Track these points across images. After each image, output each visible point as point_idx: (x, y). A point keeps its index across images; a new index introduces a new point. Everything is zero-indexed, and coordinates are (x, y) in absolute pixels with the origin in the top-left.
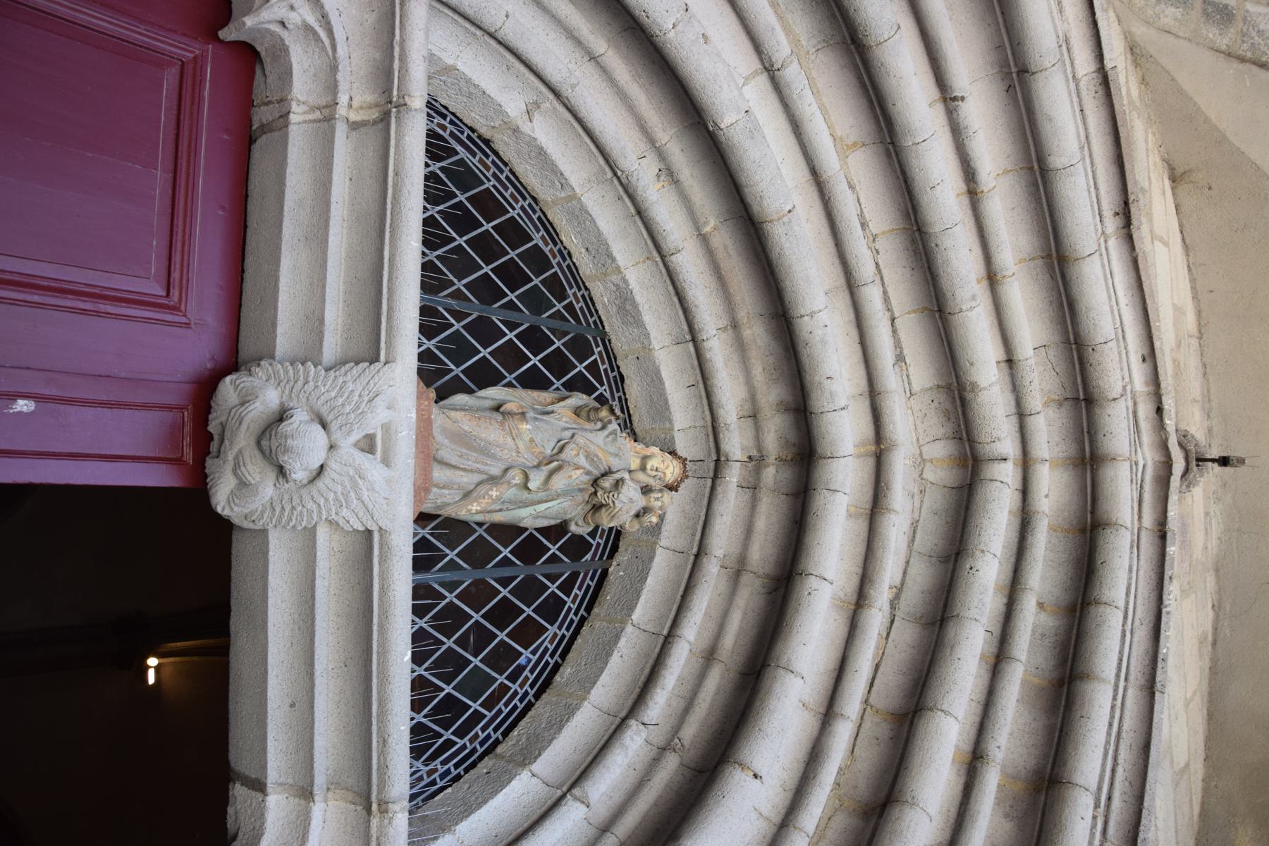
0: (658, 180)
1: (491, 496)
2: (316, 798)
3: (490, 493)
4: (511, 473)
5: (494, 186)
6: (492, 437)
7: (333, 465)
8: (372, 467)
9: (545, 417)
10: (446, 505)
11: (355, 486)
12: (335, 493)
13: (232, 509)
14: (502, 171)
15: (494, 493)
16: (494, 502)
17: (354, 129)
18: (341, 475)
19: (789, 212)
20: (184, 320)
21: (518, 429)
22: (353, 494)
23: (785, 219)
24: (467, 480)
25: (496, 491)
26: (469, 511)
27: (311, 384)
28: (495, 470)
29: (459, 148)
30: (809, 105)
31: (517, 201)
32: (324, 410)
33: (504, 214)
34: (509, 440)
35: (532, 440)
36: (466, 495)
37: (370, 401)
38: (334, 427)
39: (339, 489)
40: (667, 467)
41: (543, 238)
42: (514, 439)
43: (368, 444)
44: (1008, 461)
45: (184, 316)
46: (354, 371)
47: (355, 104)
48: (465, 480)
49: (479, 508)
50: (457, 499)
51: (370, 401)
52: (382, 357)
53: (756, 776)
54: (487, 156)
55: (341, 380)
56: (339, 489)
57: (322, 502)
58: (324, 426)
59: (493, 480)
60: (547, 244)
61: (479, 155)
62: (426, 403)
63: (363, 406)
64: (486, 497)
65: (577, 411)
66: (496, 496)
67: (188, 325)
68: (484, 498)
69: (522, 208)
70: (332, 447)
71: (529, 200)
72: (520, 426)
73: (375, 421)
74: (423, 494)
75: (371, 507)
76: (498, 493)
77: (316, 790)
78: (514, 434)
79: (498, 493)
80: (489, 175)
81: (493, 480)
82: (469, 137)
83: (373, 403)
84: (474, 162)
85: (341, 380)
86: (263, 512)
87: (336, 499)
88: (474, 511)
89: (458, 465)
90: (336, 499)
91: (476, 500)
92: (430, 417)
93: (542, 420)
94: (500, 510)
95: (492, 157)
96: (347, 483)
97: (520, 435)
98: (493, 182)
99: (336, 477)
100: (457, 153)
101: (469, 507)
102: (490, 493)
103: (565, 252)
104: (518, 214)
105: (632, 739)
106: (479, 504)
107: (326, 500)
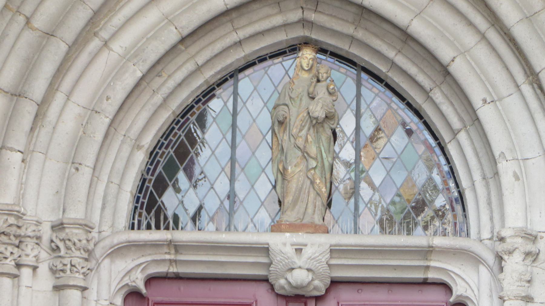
0: (161, 75)
1: (319, 183)
2: (428, 264)
3: (318, 183)
4: (310, 175)
5: (172, 148)
6: (295, 185)
7: (307, 267)
8: (308, 252)
9: (285, 151)
10: (322, 203)
11: (314, 259)
12: (316, 264)
13: (323, 290)
14: (163, 144)
15: (318, 181)
16: (321, 181)
17: (178, 251)
18: (310, 264)
19: (176, 28)
20: (254, 303)
21: (291, 173)
22: (317, 259)
23: (180, 30)
24: (312, 195)
25: (317, 180)
26: (325, 192)
27: (278, 270)
28: (308, 182)
29: (158, 171)
30: (120, 20)
31: (176, 134)
32: (287, 268)
33: (184, 142)
34: (296, 177)
35: (295, 166)
36: (318, 194)
37: (283, 253)
38: (293, 267)
39: (315, 263)
40: (307, 58)
41: (192, 115)
42: (295, 174)
43: (299, 251)
44: (308, 246)
45: (253, 303)
46: (273, 256)
47: (168, 251)
48: (312, 195)
49: (324, 188)
50: (320, 199)
51: (283, 253)
52: (267, 246)
53: (453, 61)
54: (157, 153)
55: (276, 261)
56: (315, 263)
57: (320, 267)
58: (293, 269)
59: (312, 183)
60: (194, 113)
61: (158, 158)
62: (283, 226)
63: (285, 256)
64: (319, 185)
65: (293, 259)
66: (319, 180)
67: (256, 301)
68: (320, 186)
69: (179, 129)
70: (300, 267)
71: (174, 125)
72: (290, 172)
73: (290, 251)
74: (317, 227)
75: (322, 252)
76: (318, 179)
77: (426, 264)
78: (293, 175)
79: (318, 179)
80: (167, 152)
81: (312, 183)
82: (151, 164)
83: (284, 253)
84: (163, 161)
85: (276, 261)
86: (324, 282)
87: (319, 263)
88: (325, 190)
89: (306, 203)
90: (319, 263)
91: (320, 190)
92: (288, 224)
93: (286, 153)
94: (325, 178)
95: (157, 150)
96: (313, 261)
97: (293, 172)
98: (169, 149)
99: (311, 265)
100: (160, 172)
101: (324, 192)
102: (318, 183)
103: (197, 99)
104: (183, 132)
105: (437, 98)
106: (322, 188)
107: (319, 266)
